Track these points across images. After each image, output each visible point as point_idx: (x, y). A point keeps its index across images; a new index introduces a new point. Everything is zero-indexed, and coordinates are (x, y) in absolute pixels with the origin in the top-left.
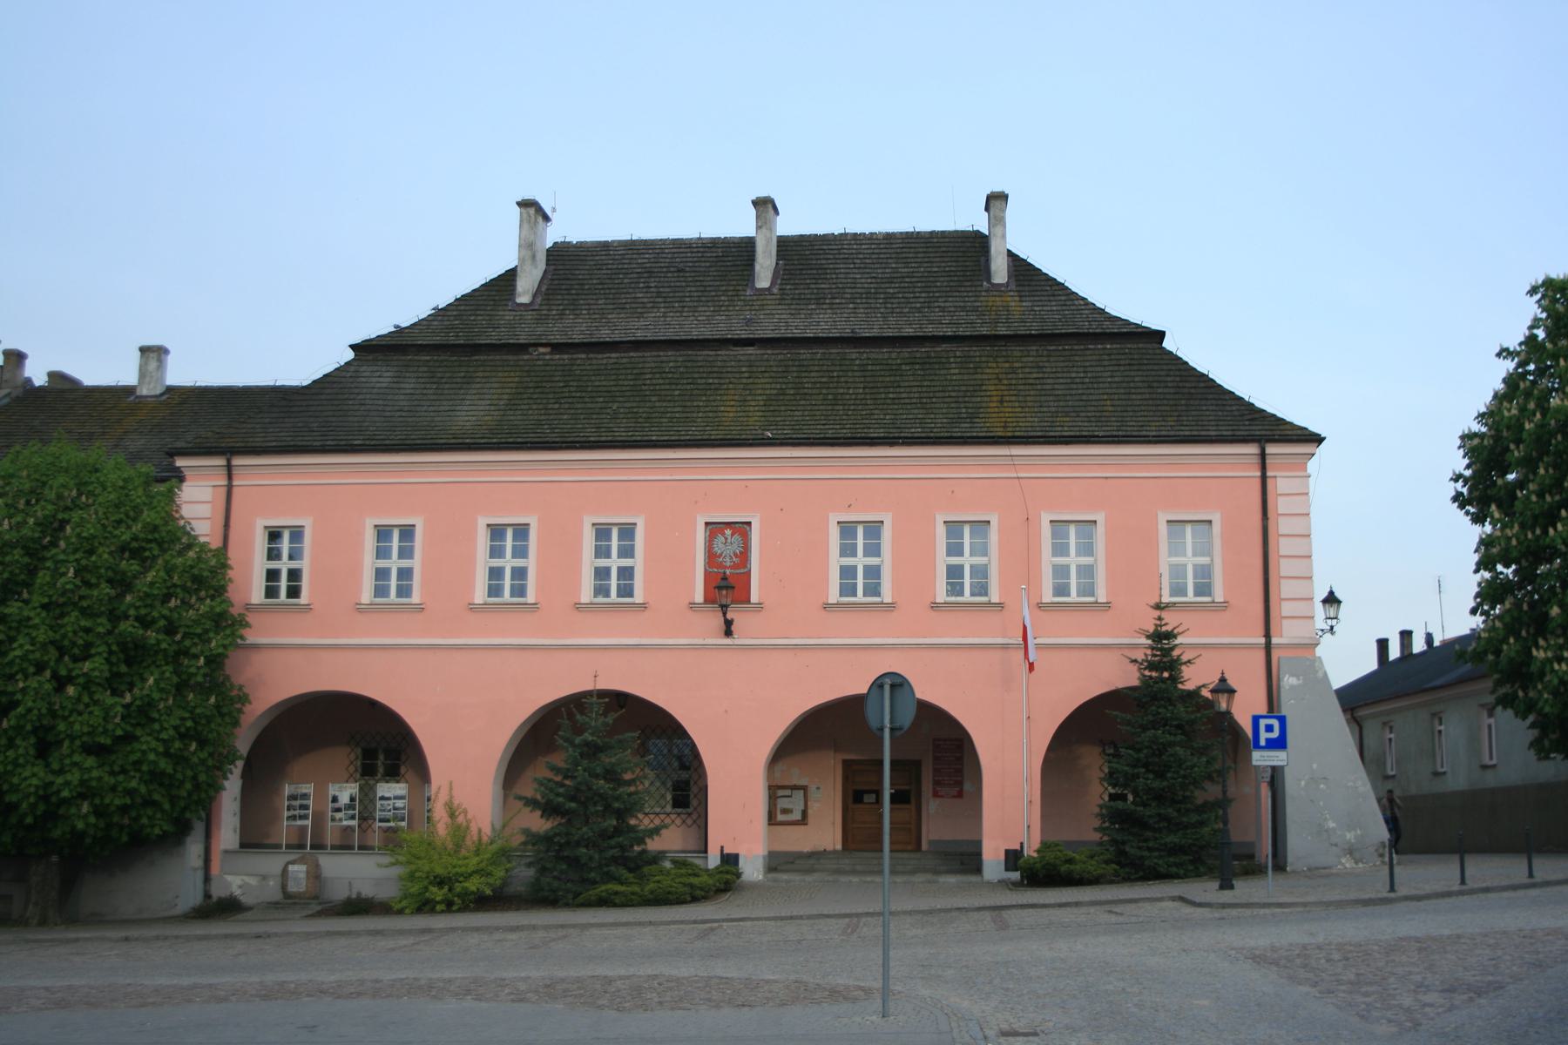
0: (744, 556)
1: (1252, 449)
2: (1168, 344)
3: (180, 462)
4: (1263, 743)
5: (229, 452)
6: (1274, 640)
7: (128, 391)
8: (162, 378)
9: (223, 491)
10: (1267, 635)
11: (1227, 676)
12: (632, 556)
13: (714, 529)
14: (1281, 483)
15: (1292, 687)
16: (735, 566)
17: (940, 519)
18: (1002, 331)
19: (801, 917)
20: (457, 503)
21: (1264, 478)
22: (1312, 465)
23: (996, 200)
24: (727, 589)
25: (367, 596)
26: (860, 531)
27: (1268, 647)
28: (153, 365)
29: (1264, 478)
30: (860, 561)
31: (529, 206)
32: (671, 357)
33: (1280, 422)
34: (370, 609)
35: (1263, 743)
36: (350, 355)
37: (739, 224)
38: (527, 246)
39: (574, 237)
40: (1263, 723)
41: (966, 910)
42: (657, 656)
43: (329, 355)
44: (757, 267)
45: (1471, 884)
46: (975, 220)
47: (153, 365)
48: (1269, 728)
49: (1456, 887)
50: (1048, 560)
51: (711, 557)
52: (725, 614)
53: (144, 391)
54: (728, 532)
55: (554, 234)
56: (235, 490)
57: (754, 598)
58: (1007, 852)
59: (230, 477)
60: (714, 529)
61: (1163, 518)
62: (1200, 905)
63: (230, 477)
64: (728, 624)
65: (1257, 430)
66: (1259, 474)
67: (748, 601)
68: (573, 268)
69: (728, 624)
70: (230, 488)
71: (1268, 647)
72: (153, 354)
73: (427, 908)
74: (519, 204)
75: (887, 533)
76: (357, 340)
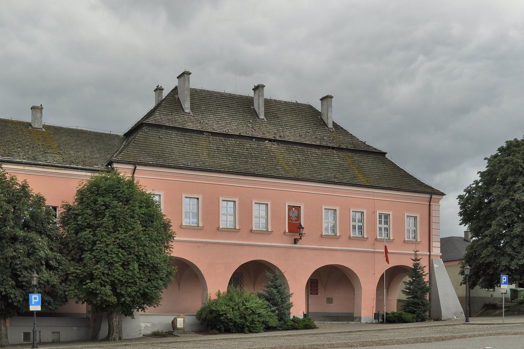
1: (428, 196)
2: (387, 156)
5: (135, 164)
13: (290, 208)
14: (434, 207)
16: (296, 221)
18: (324, 144)
21: (430, 205)
22: (441, 202)
24: (296, 228)
27: (430, 256)
28: (39, 115)
29: (430, 205)
35: (33, 303)
41: (352, 332)
42: (273, 251)
47: (39, 115)
49: (464, 322)
50: (378, 225)
51: (289, 217)
54: (294, 209)
60: (290, 208)
61: (406, 215)
71: (430, 256)
75: (418, 219)
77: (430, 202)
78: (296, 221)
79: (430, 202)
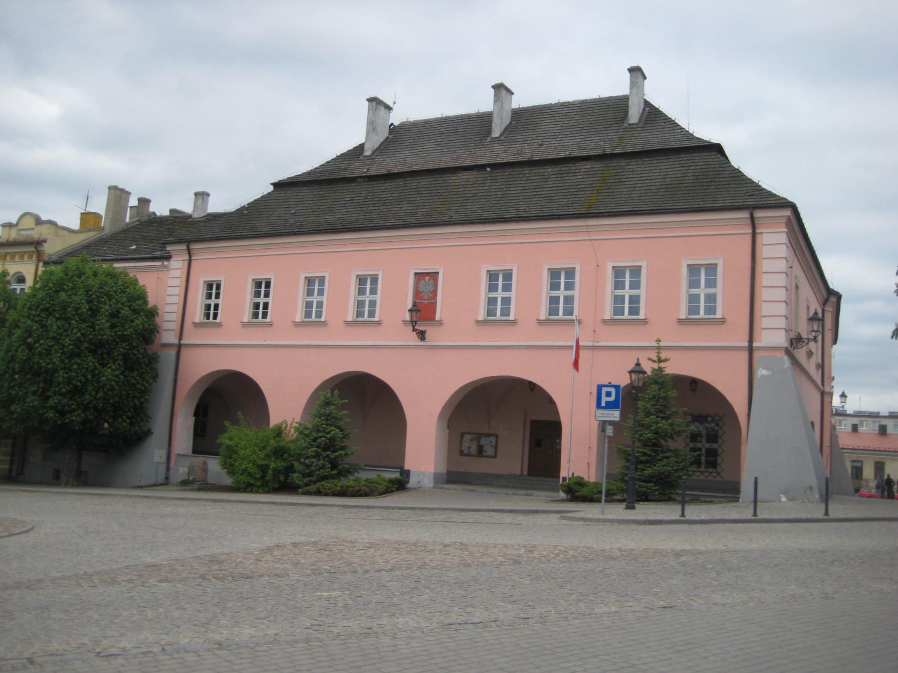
0: (435, 292)
1: (745, 215)
3: (169, 248)
4: (603, 404)
6: (755, 344)
7: (190, 216)
8: (205, 208)
9: (187, 262)
10: (751, 341)
11: (640, 362)
15: (763, 376)
19: (394, 508)
20: (288, 264)
21: (754, 235)
23: (636, 72)
24: (422, 313)
27: (751, 349)
31: (375, 102)
32: (424, 182)
33: (771, 195)
35: (603, 404)
36: (271, 188)
37: (484, 103)
40: (604, 390)
43: (259, 187)
44: (493, 125)
45: (761, 516)
46: (619, 87)
47: (200, 202)
48: (608, 394)
53: (195, 216)
54: (427, 278)
56: (193, 263)
57: (437, 318)
59: (190, 256)
63: (190, 256)
65: (751, 202)
66: (750, 231)
67: (434, 319)
68: (401, 136)
71: (751, 349)
72: (201, 196)
73: (249, 489)
74: (368, 100)
76: (276, 180)
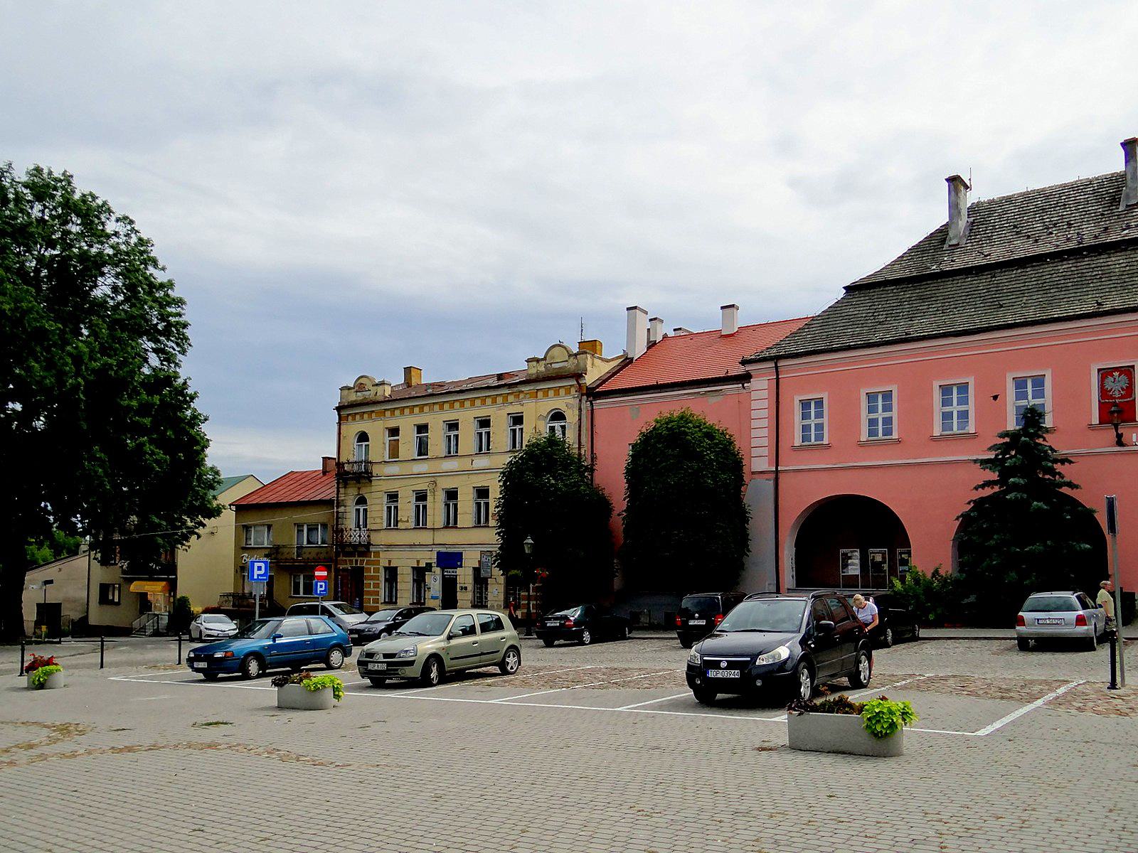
12: (967, 404)
13: (1105, 373)
16: (1122, 397)
17: (936, 385)
25: (864, 437)
26: (955, 390)
30: (880, 415)
31: (956, 183)
34: (800, 448)
38: (954, 207)
39: (985, 198)
50: (825, 420)
51: (1104, 392)
52: (1117, 430)
54: (1116, 374)
55: (971, 198)
58: (1133, 594)
60: (1105, 373)
62: (429, 636)
64: (1119, 436)
69: (1119, 436)
70: (778, 379)
74: (946, 180)
77: (778, 375)
78: (1122, 397)
79: (778, 375)
